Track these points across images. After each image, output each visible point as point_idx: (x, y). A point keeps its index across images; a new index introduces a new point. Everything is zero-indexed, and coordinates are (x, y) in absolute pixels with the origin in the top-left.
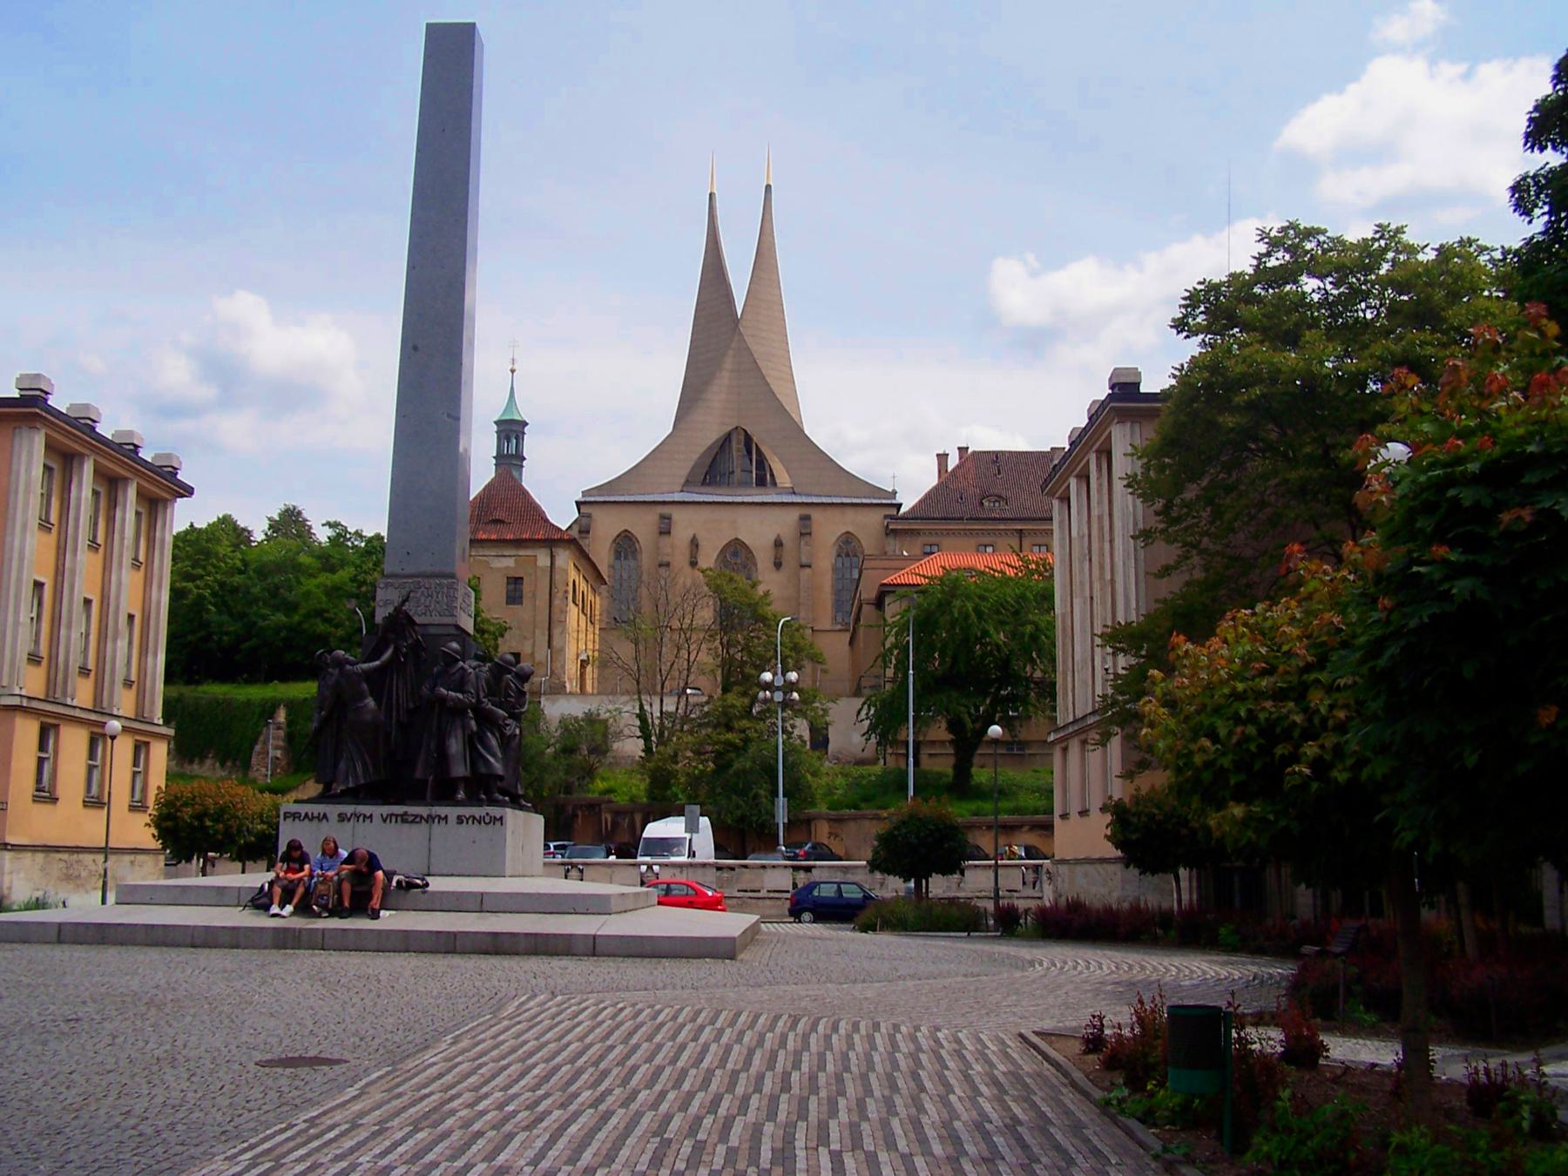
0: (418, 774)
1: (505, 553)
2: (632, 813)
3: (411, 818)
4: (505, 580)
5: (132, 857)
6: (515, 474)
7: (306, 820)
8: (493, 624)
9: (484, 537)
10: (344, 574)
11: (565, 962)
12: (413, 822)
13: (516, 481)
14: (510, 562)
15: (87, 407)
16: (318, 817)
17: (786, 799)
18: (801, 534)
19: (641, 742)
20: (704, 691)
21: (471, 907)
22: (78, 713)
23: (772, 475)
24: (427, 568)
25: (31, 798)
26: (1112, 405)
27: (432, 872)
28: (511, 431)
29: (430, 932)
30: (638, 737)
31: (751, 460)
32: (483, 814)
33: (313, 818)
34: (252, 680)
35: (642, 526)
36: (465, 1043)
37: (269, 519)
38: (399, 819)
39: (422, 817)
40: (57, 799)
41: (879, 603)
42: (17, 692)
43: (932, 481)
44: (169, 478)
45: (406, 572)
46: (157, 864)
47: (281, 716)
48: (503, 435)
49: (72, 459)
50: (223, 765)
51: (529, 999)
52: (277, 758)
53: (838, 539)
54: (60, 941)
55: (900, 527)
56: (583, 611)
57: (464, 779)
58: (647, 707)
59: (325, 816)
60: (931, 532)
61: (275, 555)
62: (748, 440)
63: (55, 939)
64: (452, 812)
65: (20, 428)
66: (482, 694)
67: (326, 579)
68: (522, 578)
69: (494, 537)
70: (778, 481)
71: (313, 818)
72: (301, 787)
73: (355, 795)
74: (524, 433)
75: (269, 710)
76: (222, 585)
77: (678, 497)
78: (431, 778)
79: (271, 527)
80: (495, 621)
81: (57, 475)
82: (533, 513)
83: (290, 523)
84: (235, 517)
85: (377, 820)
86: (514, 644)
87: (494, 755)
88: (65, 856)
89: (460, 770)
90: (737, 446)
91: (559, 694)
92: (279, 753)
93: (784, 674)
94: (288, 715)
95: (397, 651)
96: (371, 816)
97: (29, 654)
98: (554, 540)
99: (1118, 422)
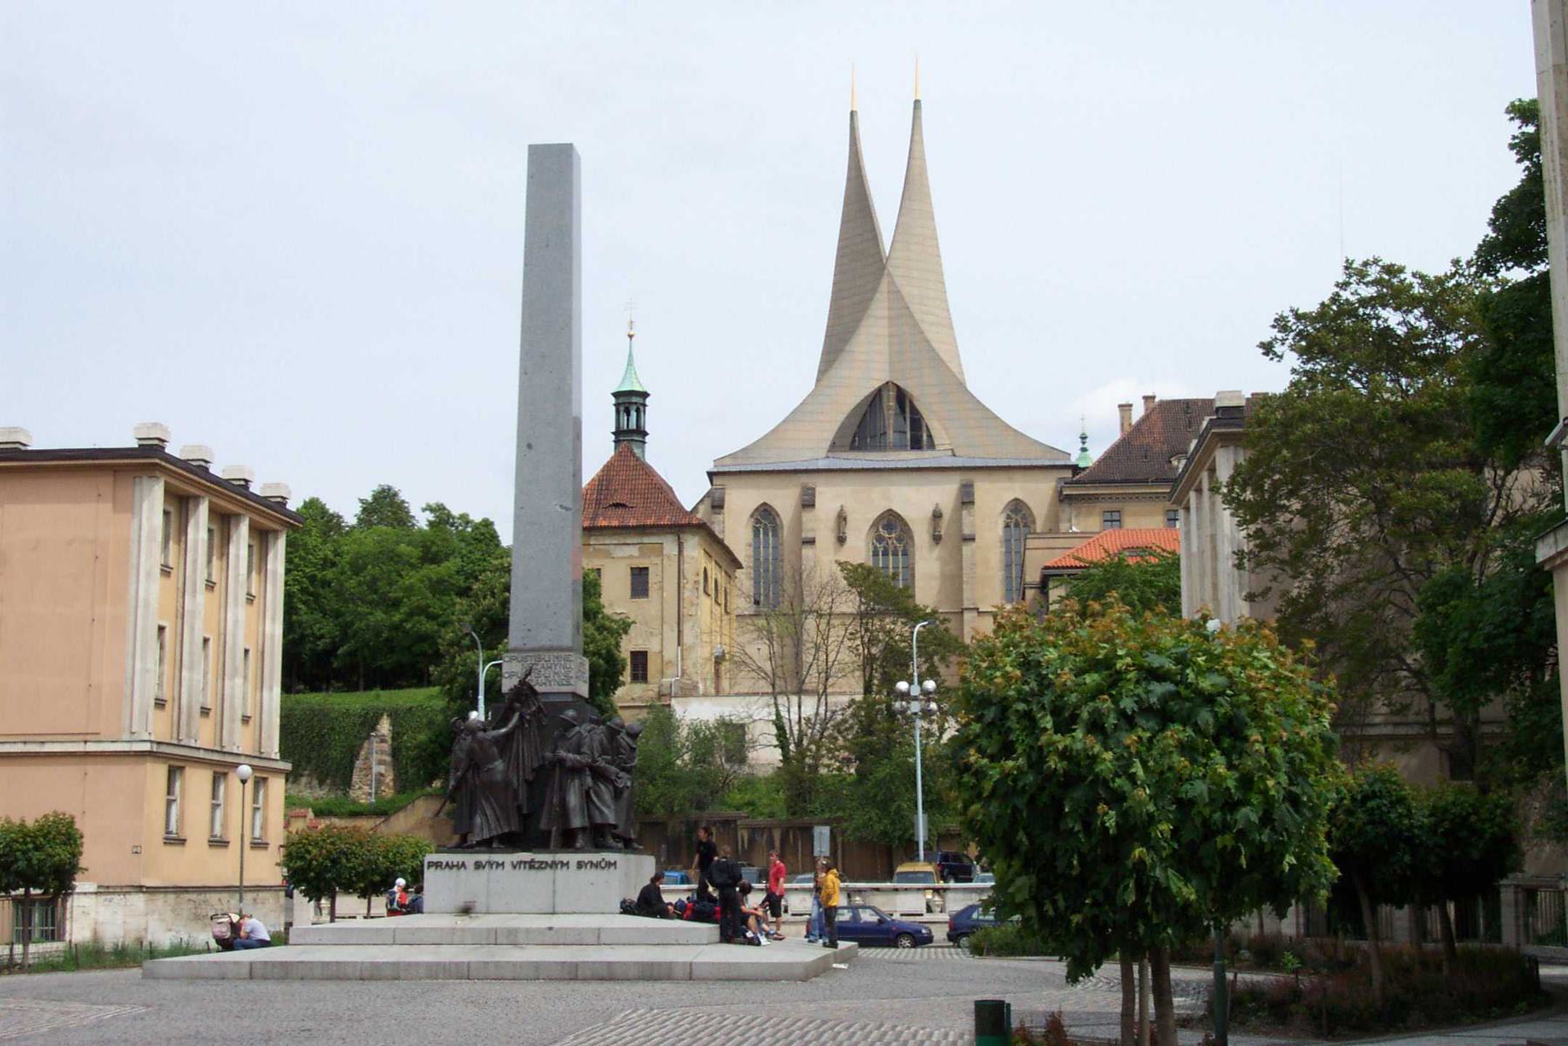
0: (543, 825)
1: (628, 542)
2: (770, 829)
3: (537, 865)
4: (629, 571)
5: (254, 895)
6: (637, 451)
7: (447, 869)
8: (616, 622)
9: (605, 523)
10: (452, 565)
11: (667, 986)
12: (539, 868)
13: (638, 459)
14: (634, 551)
15: (200, 447)
16: (457, 866)
17: (926, 816)
18: (963, 503)
19: (779, 751)
20: (847, 691)
21: (589, 942)
22: (201, 754)
23: (930, 436)
24: (545, 642)
25: (162, 841)
26: (1213, 431)
27: (557, 910)
28: (630, 402)
29: (556, 963)
30: (775, 746)
31: (905, 419)
32: (600, 859)
33: (453, 866)
34: (352, 687)
35: (784, 500)
36: (581, 1039)
37: (361, 501)
38: (527, 866)
39: (547, 863)
40: (185, 840)
41: (1043, 587)
42: (147, 738)
43: (1115, 436)
44: (278, 508)
45: (528, 646)
46: (278, 901)
47: (385, 727)
48: (622, 408)
49: (188, 503)
50: (321, 783)
51: (633, 1012)
52: (382, 775)
53: (1005, 508)
54: (251, 977)
55: (1075, 493)
56: (716, 601)
57: (583, 829)
58: (784, 713)
59: (463, 864)
60: (1110, 497)
61: (370, 541)
62: (902, 397)
63: (247, 976)
64: (573, 858)
65: (141, 477)
66: (596, 755)
67: (432, 571)
68: (647, 569)
69: (615, 523)
70: (936, 443)
71: (453, 866)
72: (409, 807)
73: (487, 845)
74: (645, 405)
75: (369, 723)
76: (312, 579)
77: (822, 464)
78: (554, 829)
79: (364, 510)
80: (617, 618)
81: (173, 518)
82: (660, 492)
83: (385, 506)
84: (323, 500)
85: (508, 866)
86: (640, 641)
87: (608, 807)
88: (194, 896)
89: (577, 822)
90: (890, 402)
91: (691, 696)
92: (382, 769)
93: (920, 683)
94: (393, 724)
95: (521, 717)
96: (503, 863)
97: (156, 699)
98: (683, 526)
99: (1222, 447)
